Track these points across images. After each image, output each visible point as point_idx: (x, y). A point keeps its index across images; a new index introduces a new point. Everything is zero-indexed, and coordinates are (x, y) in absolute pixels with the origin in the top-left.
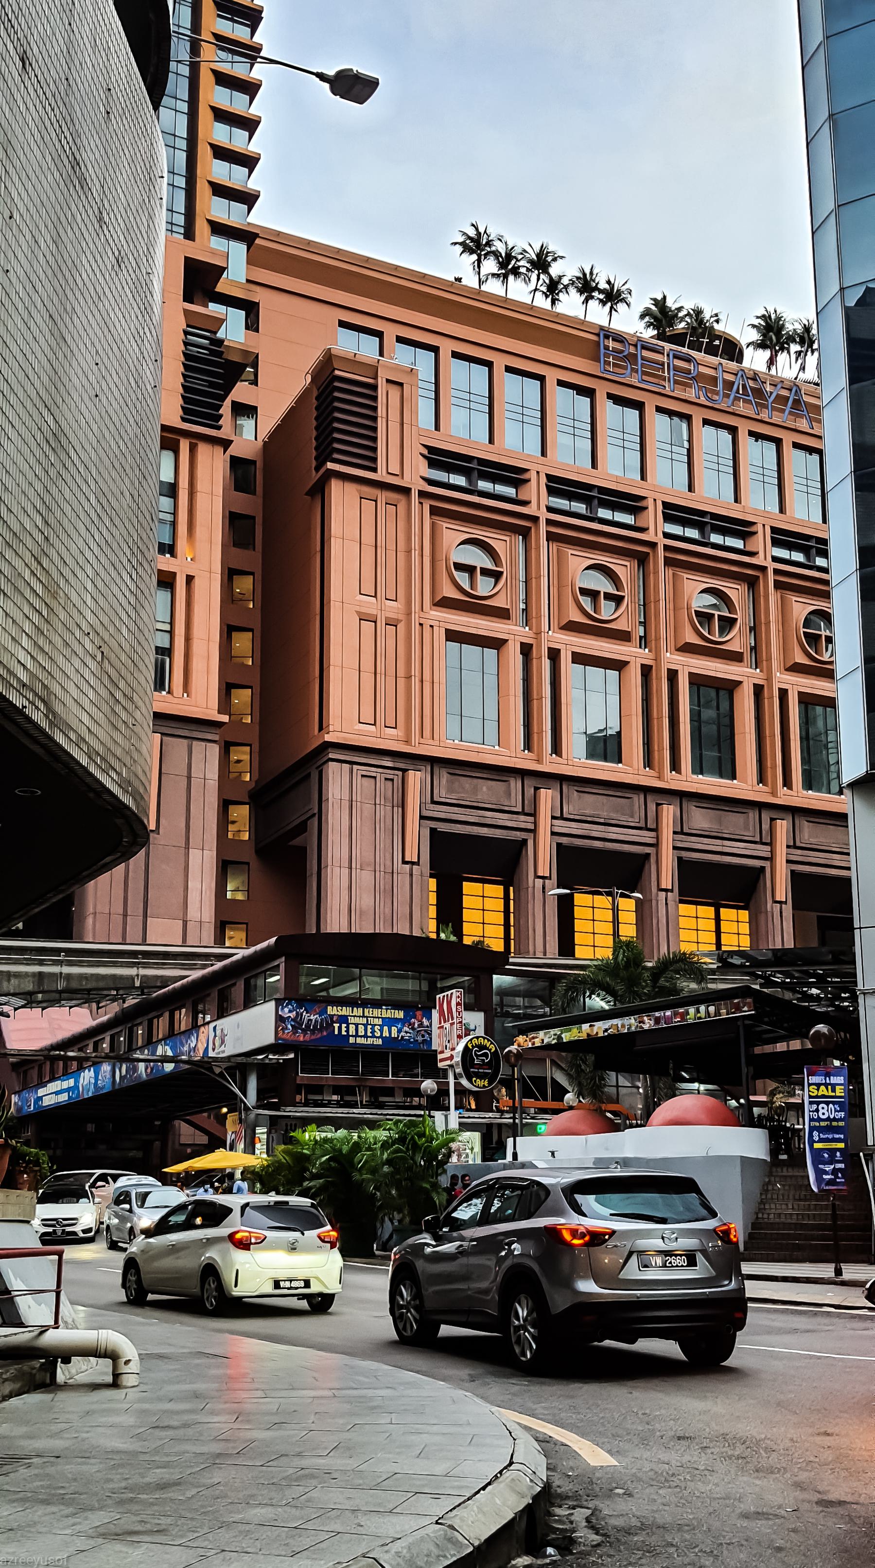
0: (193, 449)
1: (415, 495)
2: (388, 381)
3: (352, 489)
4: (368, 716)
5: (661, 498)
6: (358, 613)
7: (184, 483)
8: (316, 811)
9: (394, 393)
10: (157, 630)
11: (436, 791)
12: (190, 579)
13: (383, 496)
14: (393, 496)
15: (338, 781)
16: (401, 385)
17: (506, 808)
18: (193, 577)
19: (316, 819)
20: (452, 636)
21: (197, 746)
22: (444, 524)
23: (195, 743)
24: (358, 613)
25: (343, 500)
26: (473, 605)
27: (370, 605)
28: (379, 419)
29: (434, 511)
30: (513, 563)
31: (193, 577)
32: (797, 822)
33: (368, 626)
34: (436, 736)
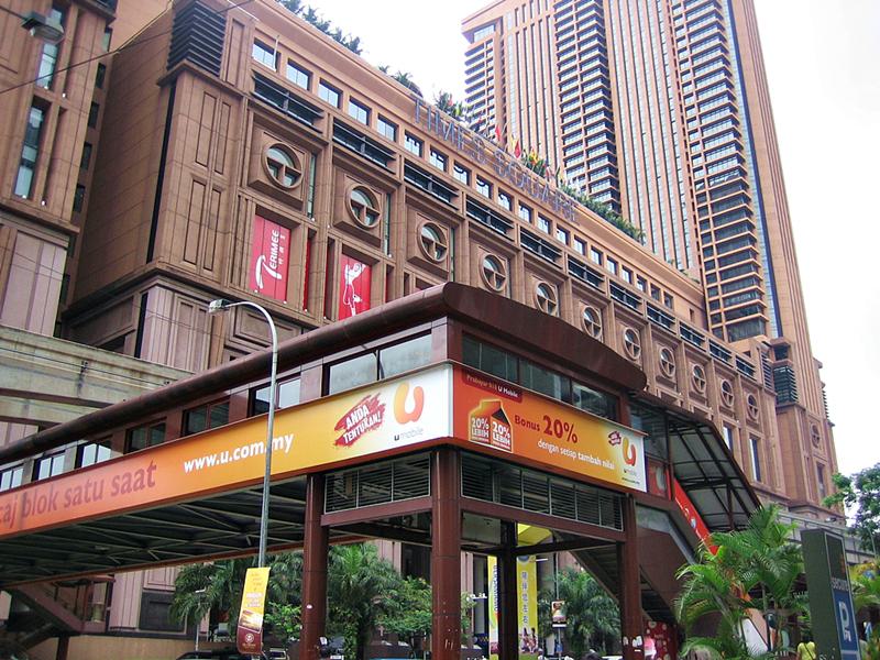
0: (80, 15)
1: (245, 101)
2: (209, 367)
3: (200, 86)
4: (191, 255)
5: (404, 156)
6: (193, 175)
7: (69, 36)
8: (136, 327)
9: (237, 32)
10: (16, 73)
11: (237, 328)
12: (62, 111)
13: (222, 97)
14: (229, 100)
15: (160, 301)
16: (242, 26)
17: (303, 282)
18: (65, 110)
19: (135, 334)
20: (262, 212)
21: (48, 249)
22: (261, 132)
23: (46, 245)
24: (193, 175)
25: (190, 94)
26: (279, 194)
27: (202, 172)
28: (221, 71)
29: (256, 119)
30: (307, 171)
31: (65, 110)
32: (521, 366)
33: (198, 188)
34: (242, 285)
